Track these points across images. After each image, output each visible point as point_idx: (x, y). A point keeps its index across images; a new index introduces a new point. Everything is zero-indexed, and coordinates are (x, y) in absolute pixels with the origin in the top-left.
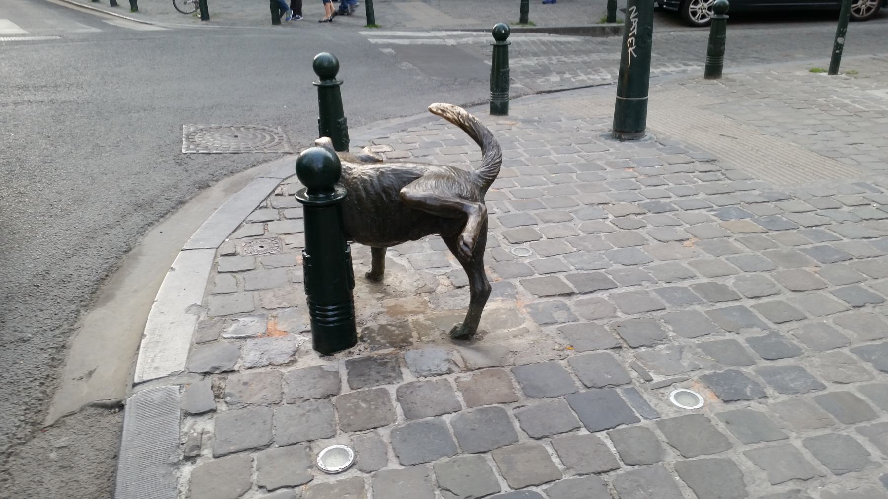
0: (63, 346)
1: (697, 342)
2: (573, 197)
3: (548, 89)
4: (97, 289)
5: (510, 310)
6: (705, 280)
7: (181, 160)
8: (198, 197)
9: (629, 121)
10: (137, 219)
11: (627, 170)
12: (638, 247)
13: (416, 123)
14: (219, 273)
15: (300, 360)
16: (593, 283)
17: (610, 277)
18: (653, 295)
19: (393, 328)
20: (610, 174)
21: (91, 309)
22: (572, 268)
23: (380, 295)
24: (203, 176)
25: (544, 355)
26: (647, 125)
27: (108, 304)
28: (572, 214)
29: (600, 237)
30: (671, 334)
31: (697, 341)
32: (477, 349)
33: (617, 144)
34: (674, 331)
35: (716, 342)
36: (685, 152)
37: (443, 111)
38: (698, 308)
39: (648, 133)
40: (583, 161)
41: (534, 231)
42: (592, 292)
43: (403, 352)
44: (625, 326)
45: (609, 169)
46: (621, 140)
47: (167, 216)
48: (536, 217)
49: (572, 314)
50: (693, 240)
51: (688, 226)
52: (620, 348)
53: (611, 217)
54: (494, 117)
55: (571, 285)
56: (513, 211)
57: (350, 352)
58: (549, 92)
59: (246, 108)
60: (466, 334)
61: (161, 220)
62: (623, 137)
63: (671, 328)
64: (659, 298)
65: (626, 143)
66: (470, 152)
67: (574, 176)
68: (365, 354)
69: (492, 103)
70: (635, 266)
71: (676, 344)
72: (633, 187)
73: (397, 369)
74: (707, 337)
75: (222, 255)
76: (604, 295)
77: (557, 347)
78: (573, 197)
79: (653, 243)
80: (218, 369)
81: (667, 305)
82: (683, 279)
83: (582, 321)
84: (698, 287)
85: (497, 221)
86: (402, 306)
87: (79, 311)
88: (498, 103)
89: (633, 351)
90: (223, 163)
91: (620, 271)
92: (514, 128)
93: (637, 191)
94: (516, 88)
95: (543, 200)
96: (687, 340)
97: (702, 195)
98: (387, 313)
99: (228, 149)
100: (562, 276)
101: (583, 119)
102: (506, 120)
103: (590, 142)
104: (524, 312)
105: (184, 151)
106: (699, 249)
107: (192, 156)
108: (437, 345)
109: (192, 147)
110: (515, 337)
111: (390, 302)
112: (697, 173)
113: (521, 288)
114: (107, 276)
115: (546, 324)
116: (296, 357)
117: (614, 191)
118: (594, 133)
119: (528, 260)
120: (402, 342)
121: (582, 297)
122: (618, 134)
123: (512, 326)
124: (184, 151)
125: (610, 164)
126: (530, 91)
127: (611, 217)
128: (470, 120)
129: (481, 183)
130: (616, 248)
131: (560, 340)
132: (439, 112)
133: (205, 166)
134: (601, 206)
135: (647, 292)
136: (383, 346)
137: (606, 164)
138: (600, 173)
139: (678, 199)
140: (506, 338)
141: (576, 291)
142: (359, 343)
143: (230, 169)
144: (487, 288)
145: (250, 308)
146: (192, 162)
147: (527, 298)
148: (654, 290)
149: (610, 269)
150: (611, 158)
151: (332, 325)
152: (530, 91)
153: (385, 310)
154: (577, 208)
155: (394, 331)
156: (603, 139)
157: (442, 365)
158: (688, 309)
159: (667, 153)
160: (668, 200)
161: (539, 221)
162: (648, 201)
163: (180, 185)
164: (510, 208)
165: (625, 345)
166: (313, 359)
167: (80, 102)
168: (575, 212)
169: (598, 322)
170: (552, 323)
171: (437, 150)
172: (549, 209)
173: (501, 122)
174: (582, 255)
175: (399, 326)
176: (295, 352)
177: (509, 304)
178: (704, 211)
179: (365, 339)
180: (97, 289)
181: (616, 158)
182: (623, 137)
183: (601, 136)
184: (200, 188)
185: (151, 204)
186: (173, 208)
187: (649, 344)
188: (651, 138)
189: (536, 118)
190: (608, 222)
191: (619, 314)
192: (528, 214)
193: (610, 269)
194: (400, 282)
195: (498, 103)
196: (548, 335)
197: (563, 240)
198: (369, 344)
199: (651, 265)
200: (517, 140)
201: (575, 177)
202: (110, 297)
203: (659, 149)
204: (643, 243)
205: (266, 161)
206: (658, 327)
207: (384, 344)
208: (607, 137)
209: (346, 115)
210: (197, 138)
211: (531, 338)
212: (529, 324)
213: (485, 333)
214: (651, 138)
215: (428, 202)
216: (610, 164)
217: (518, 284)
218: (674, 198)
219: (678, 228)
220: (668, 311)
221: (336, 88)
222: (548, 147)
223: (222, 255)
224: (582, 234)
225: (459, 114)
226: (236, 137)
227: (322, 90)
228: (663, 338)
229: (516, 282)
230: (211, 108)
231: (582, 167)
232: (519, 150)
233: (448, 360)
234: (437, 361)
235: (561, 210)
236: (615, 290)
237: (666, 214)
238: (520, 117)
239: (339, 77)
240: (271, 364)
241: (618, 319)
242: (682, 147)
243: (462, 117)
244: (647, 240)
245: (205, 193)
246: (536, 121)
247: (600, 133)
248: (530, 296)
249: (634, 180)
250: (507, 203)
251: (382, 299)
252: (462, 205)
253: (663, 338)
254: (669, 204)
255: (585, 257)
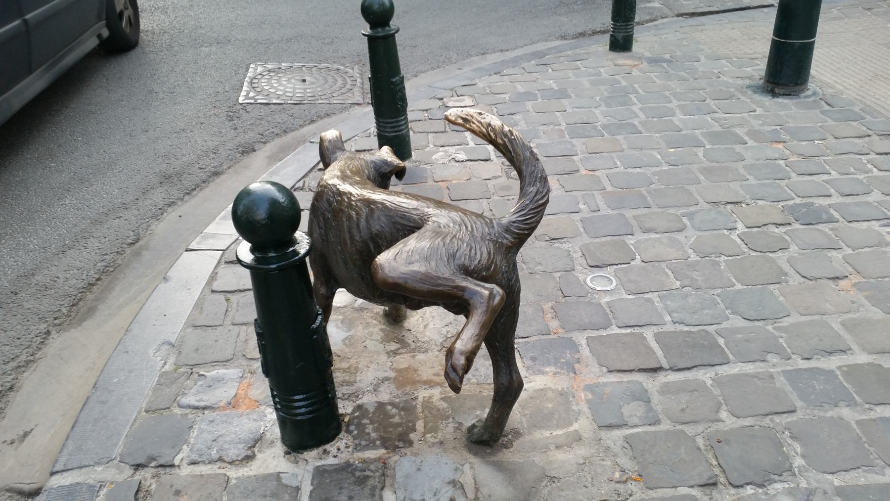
0: (11, 388)
1: (836, 483)
2: (692, 188)
3: (692, 11)
4: (80, 300)
5: (562, 394)
6: (862, 358)
7: (234, 112)
8: (237, 166)
9: (787, 68)
10: (158, 197)
11: (775, 145)
12: (772, 287)
13: (515, 62)
14: (213, 291)
15: (259, 456)
16: (695, 351)
17: (721, 341)
18: (781, 382)
19: (394, 411)
20: (751, 151)
21: (65, 330)
22: (668, 318)
23: (394, 346)
24: (251, 136)
25: (594, 490)
26: (813, 72)
27: (85, 324)
28: (685, 220)
29: (718, 264)
30: (798, 462)
31: (837, 481)
32: (500, 467)
33: (767, 100)
34: (803, 456)
35: (867, 487)
36: (858, 118)
37: (465, 120)
38: (845, 412)
39: (811, 85)
40: (717, 128)
41: (625, 245)
42: (689, 369)
43: (396, 458)
44: (728, 442)
45: (750, 143)
46: (774, 95)
47: (195, 193)
48: (633, 222)
49: (651, 409)
50: (855, 278)
51: (850, 251)
52: (714, 484)
53: (741, 227)
54: (614, 55)
55: (659, 353)
56: (605, 211)
57: (325, 451)
58: (693, 15)
59: (327, 41)
60: (489, 438)
61: (186, 198)
62: (777, 90)
63: (799, 450)
64: (788, 388)
65: (780, 100)
66: (569, 110)
67: (700, 152)
68: (344, 457)
69: (612, 36)
70: (761, 323)
71: (804, 485)
72: (780, 176)
73: (377, 492)
74: (854, 474)
75: (226, 263)
76: (705, 376)
77: (617, 475)
78: (692, 188)
79: (795, 280)
80: (154, 459)
81: (799, 404)
82: (830, 353)
83: (666, 426)
84: (852, 371)
85: (580, 225)
86: (416, 370)
87: (48, 333)
88: (620, 36)
89: (733, 491)
90: (278, 118)
91: (738, 330)
92: (635, 72)
93: (783, 183)
94: (652, 8)
95: (648, 192)
96: (821, 476)
97: (876, 196)
98: (395, 378)
99: (291, 98)
100: (649, 334)
101: (728, 59)
102: (628, 58)
103: (731, 97)
104: (581, 402)
105: (241, 100)
106: (861, 298)
107: (249, 108)
108: (445, 451)
109: (251, 94)
110: (558, 447)
111: (403, 361)
112: (873, 156)
113: (585, 352)
114: (98, 280)
115: (610, 427)
116: (256, 450)
117: (752, 181)
118: (740, 82)
119: (607, 299)
120: (397, 438)
121: (673, 377)
122: (771, 86)
123: (558, 427)
124: (241, 100)
125: (755, 134)
126: (669, 13)
127: (740, 227)
128: (506, 135)
129: (508, 239)
130: (739, 286)
131: (625, 461)
132: (460, 121)
133: (258, 122)
134: (729, 207)
135: (771, 377)
136: (371, 445)
137: (748, 134)
138: (738, 148)
139: (841, 200)
140: (545, 449)
141: (665, 365)
142: (343, 434)
143: (284, 126)
144: (516, 385)
145: (228, 354)
146: (245, 116)
147: (592, 372)
148: (784, 372)
149: (725, 325)
150: (756, 124)
151: (299, 418)
152: (669, 13)
153: (392, 374)
154: (693, 209)
155: (393, 416)
156: (750, 92)
157: (443, 491)
158: (829, 414)
159: (835, 120)
160: (824, 202)
161: (636, 229)
162: (798, 201)
163: (221, 149)
164: (602, 204)
165: (722, 479)
166: (273, 459)
167: (157, 31)
168: (690, 216)
169: (689, 430)
170: (619, 426)
171: (529, 105)
172: (655, 209)
173: (620, 62)
174: (686, 296)
175: (403, 409)
176: (256, 441)
177: (562, 383)
178: (875, 225)
179: (352, 428)
180: (80, 300)
181: (762, 125)
182: (777, 90)
183: (748, 87)
184: (243, 153)
185: (180, 175)
186: (204, 182)
187: (759, 481)
188: (815, 94)
189: (668, 56)
190: (734, 236)
191: (724, 414)
192: (623, 216)
193: (725, 325)
194: (425, 327)
195: (620, 36)
196: (608, 449)
197: (663, 265)
198: (355, 438)
199: (786, 322)
200: (635, 91)
201: (701, 154)
202: (91, 311)
203: (824, 112)
204: (779, 278)
205: (328, 115)
206: (779, 445)
207: (374, 442)
208: (756, 89)
209: (403, 72)
210: (264, 83)
211: (581, 452)
212: (583, 425)
213: (517, 434)
214: (815, 94)
215: (411, 284)
216: (755, 134)
217: (584, 342)
218: (836, 199)
219: (834, 253)
220: (799, 414)
221: (390, 39)
222: (675, 103)
223: (226, 263)
224: (693, 257)
225: (489, 125)
226: (304, 81)
227: (372, 40)
228: (783, 469)
229: (581, 339)
230: (289, 40)
231: (714, 137)
232: (635, 108)
233: (454, 483)
234: (437, 484)
235: (671, 211)
236: (725, 367)
237: (820, 227)
238: (647, 54)
239: (394, 23)
240: (221, 459)
241: (720, 426)
242: (856, 109)
243: (494, 130)
244: (786, 274)
245: (247, 160)
246: (665, 61)
247: (748, 82)
248: (596, 368)
249: (782, 162)
250: (598, 196)
251: (395, 353)
252: (463, 289)
253: (783, 469)
254: (825, 209)
255: (690, 300)
